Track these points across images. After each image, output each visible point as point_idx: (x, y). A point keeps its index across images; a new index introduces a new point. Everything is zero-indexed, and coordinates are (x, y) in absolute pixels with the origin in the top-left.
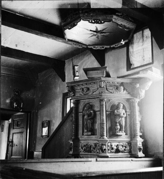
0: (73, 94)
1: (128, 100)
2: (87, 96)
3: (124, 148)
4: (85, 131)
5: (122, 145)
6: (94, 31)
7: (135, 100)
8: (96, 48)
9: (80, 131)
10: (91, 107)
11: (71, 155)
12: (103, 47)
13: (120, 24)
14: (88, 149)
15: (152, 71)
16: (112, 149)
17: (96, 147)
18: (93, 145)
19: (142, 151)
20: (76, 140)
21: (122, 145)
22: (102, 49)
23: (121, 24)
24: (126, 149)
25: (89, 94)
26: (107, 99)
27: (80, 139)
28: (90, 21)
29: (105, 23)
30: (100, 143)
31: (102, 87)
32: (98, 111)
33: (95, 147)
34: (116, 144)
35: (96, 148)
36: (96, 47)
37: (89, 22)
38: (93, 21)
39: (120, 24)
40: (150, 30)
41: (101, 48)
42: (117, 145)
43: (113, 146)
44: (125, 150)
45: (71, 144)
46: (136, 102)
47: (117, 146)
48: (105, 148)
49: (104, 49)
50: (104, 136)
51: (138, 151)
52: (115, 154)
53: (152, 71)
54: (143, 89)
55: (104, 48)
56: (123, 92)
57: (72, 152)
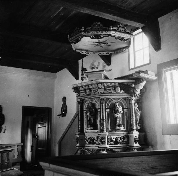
0: (78, 95)
1: (125, 99)
2: (89, 96)
3: (122, 140)
4: (89, 126)
5: (120, 138)
6: (97, 43)
7: (132, 98)
8: (102, 54)
9: (85, 126)
10: (93, 105)
11: (30, 137)
12: (108, 53)
13: (118, 37)
14: (92, 142)
15: (148, 74)
16: (112, 141)
17: (98, 140)
18: (96, 138)
19: (138, 142)
20: (82, 131)
21: (120, 138)
22: (107, 54)
23: (119, 37)
24: (125, 141)
25: (91, 94)
26: (107, 98)
27: (85, 133)
28: (92, 37)
29: (105, 37)
30: (100, 137)
31: (101, 88)
32: (99, 109)
33: (97, 139)
34: (115, 136)
35: (98, 140)
36: (102, 53)
37: (91, 38)
38: (94, 37)
39: (118, 37)
40: (79, 60)
41: (106, 54)
42: (116, 138)
43: (112, 139)
44: (123, 142)
45: (78, 137)
46: (133, 100)
47: (115, 139)
48: (104, 141)
49: (109, 55)
50: (104, 130)
51: (134, 143)
52: (114, 145)
53: (148, 74)
54: (138, 88)
55: (109, 54)
56: (120, 91)
57: (79, 144)
